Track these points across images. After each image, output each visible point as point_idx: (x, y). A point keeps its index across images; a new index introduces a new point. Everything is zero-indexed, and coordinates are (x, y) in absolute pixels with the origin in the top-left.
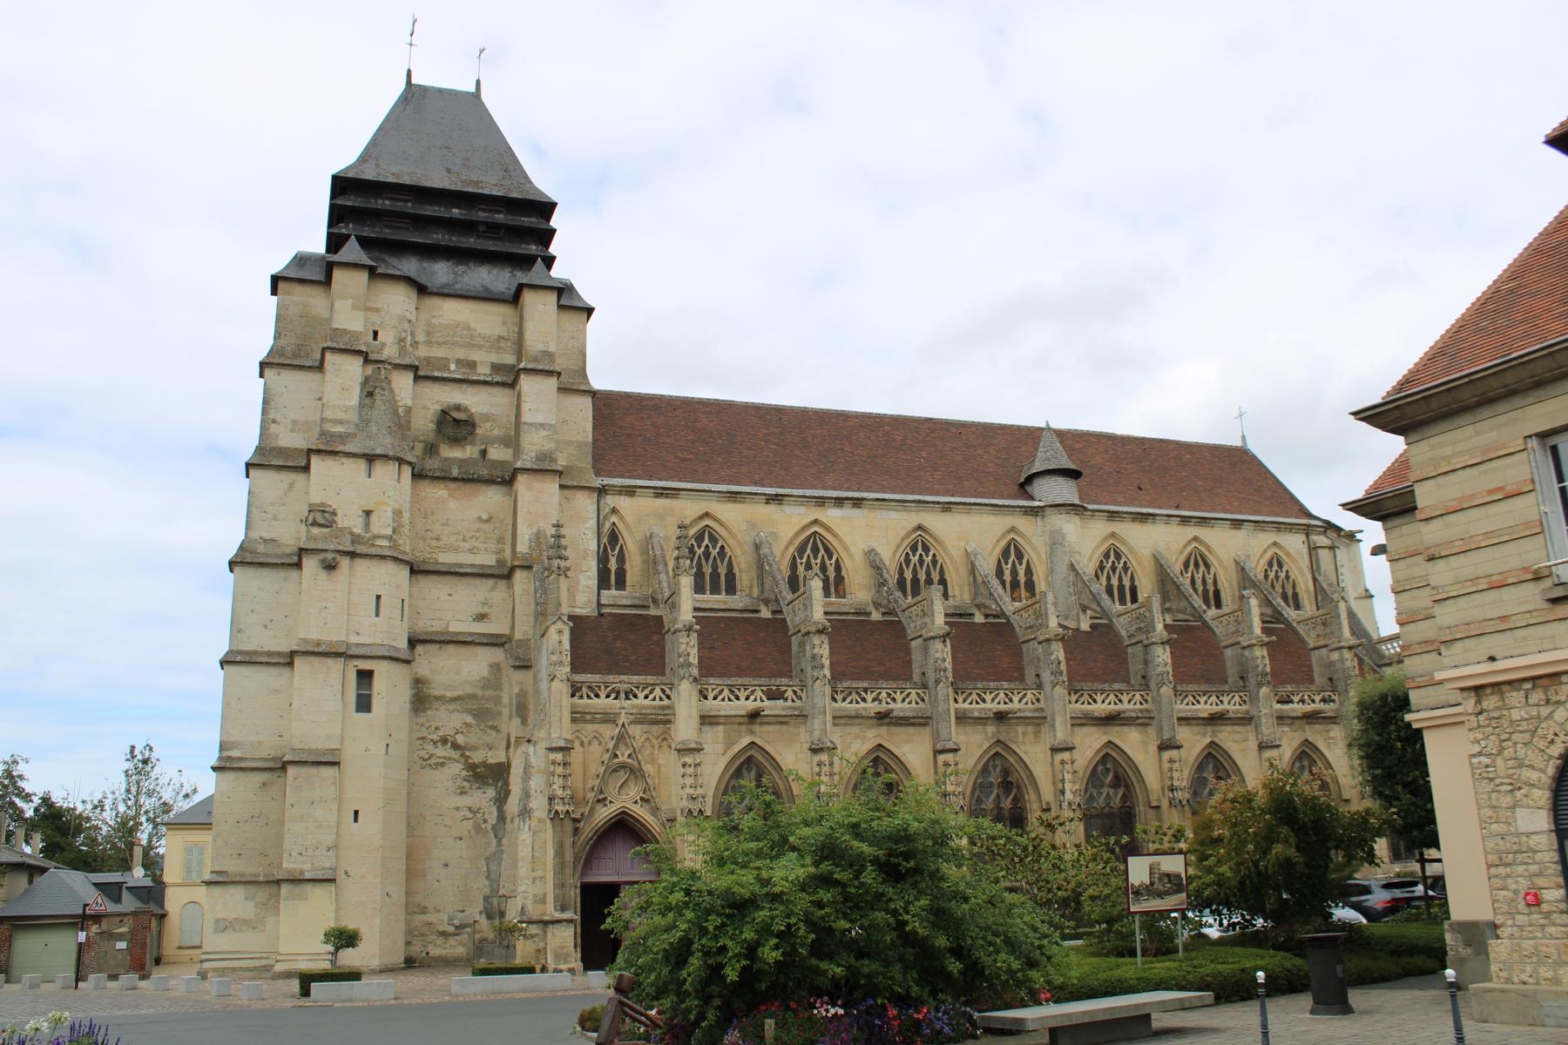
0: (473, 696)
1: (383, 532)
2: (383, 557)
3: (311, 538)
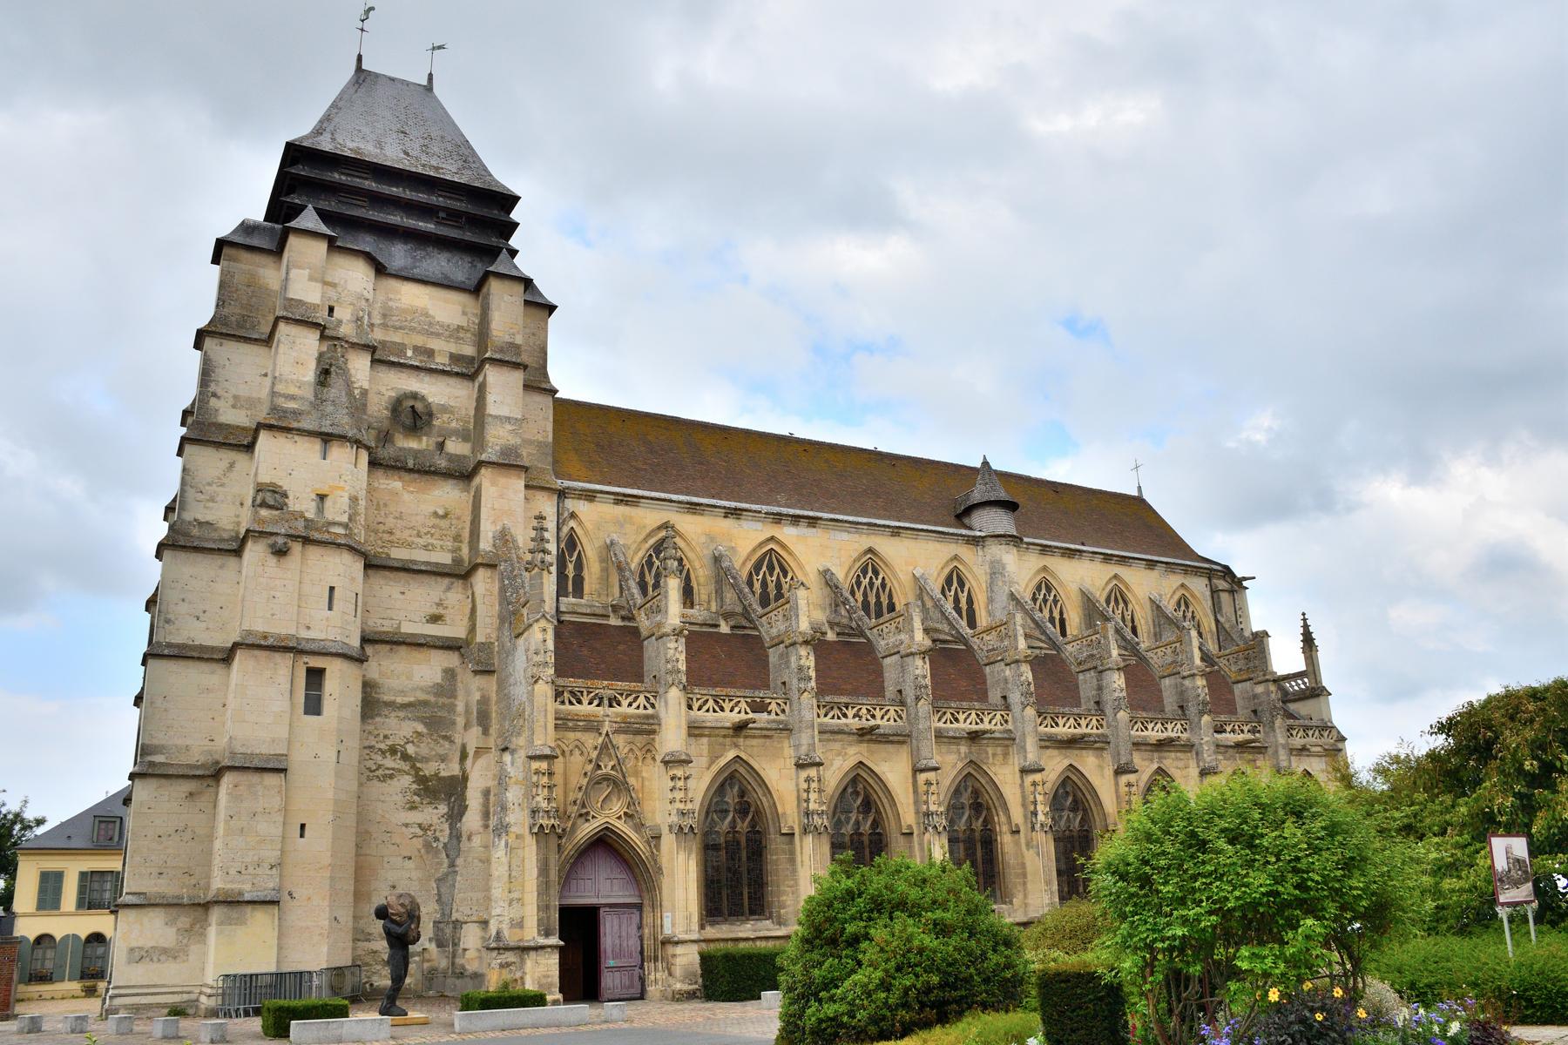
0: (425, 703)
1: (337, 519)
2: (339, 545)
3: (257, 519)
